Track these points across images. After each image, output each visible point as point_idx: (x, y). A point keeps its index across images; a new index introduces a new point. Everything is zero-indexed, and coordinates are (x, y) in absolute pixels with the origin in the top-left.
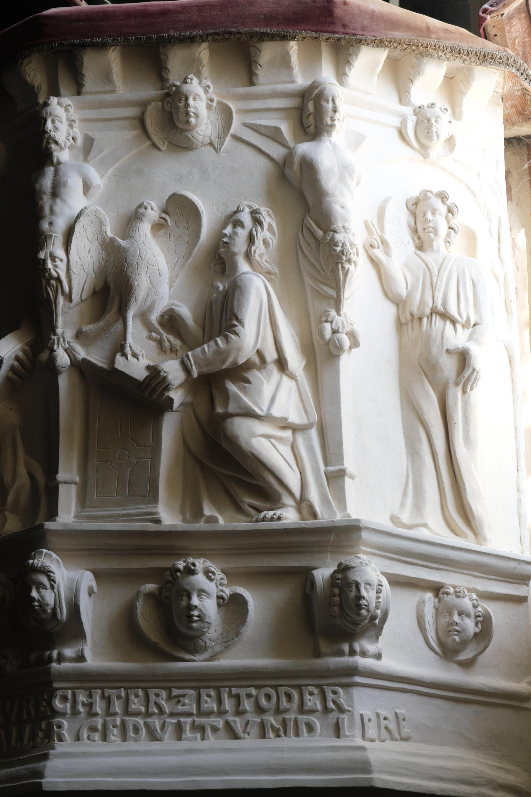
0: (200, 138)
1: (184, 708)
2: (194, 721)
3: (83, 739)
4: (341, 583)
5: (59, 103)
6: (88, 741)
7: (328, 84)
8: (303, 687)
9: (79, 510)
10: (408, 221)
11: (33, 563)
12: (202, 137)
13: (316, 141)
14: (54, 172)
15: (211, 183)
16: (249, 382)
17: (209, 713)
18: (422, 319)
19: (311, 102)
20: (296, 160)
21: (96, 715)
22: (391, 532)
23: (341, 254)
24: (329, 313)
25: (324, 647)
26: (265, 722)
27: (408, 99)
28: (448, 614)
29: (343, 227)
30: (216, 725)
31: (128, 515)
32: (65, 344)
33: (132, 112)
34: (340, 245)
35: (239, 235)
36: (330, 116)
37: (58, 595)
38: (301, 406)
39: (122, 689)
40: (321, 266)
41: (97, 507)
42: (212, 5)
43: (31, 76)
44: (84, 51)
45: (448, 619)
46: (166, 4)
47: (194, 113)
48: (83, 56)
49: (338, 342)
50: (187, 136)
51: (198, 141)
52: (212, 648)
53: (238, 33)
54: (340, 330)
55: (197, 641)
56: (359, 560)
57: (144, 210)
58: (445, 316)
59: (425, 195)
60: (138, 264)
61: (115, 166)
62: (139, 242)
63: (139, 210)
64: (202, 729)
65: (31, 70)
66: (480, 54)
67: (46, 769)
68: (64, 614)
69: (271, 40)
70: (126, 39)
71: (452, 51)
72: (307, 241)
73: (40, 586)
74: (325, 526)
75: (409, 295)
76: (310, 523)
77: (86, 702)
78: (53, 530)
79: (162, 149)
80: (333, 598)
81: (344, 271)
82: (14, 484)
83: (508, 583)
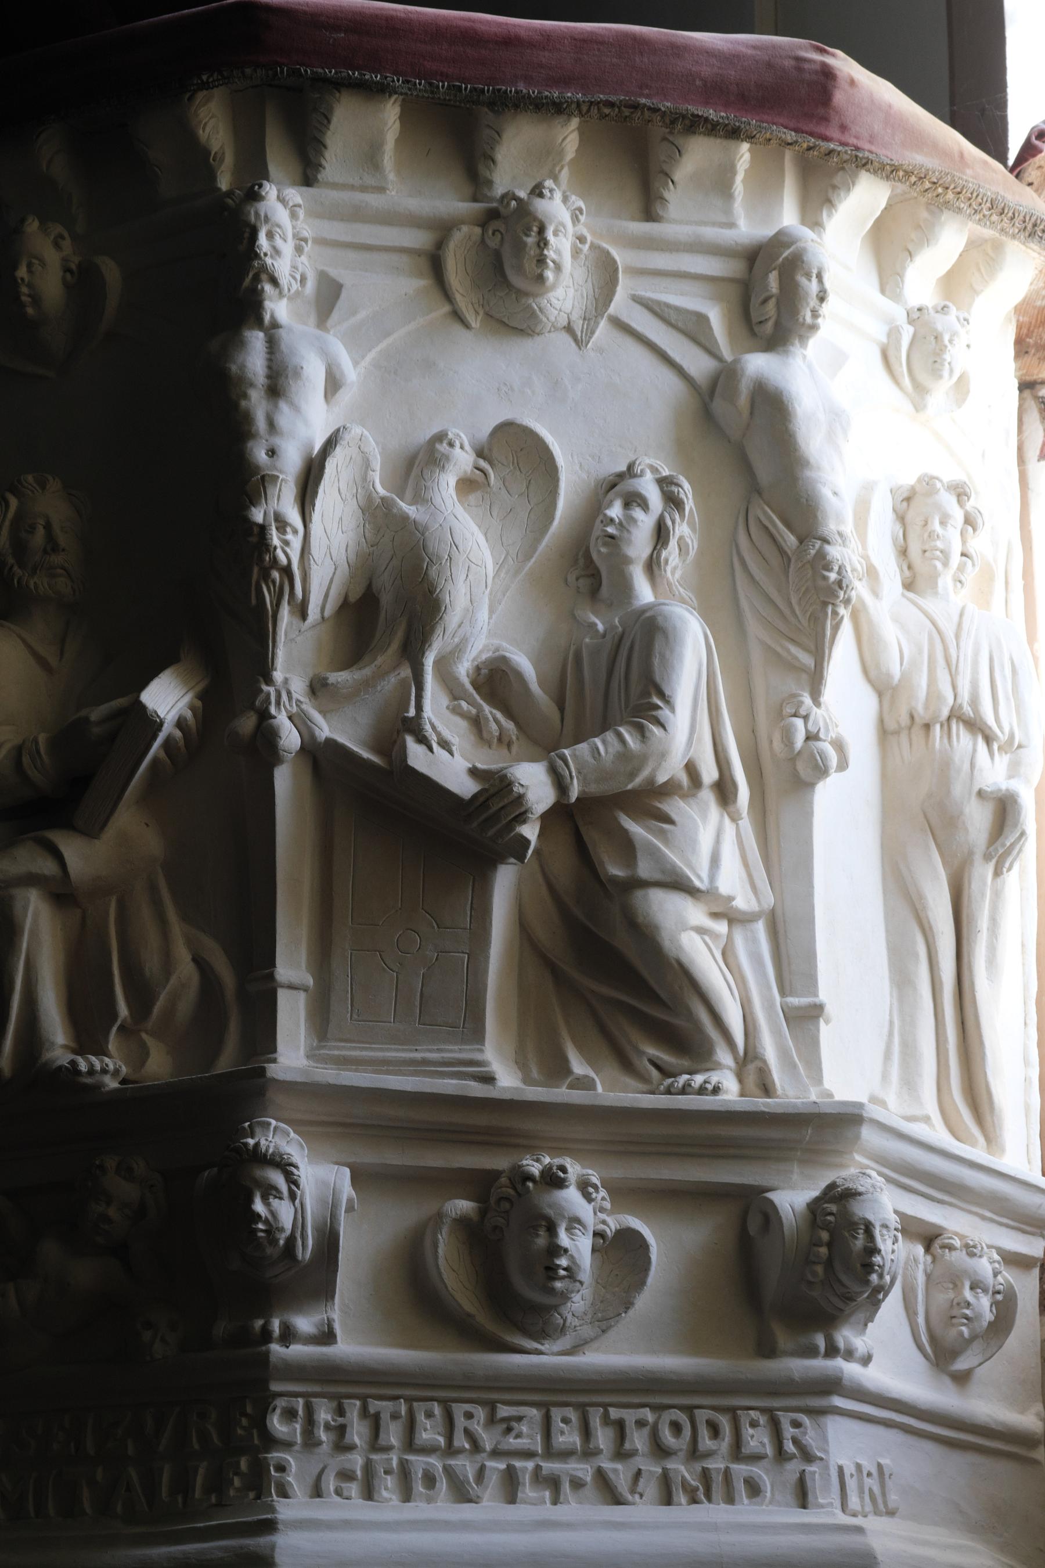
0: (553, 314)
1: (519, 1443)
2: (538, 1468)
3: (329, 1495)
4: (836, 1221)
5: (281, 198)
6: (337, 1499)
7: (810, 241)
8: (739, 1412)
9: (315, 1044)
10: (892, 532)
11: (257, 1144)
12: (557, 312)
13: (778, 353)
14: (266, 342)
15: (569, 408)
16: (670, 821)
17: (566, 1454)
18: (931, 728)
19: (774, 272)
20: (745, 388)
21: (351, 1448)
22: (901, 1129)
23: (837, 588)
24: (801, 698)
25: (783, 1339)
26: (671, 1475)
27: (898, 290)
28: (951, 1286)
29: (838, 532)
30: (581, 1476)
31: (425, 1062)
32: (291, 706)
33: (418, 239)
34: (836, 568)
35: (639, 523)
36: (812, 307)
37: (300, 1213)
38: (744, 875)
39: (402, 1400)
40: (790, 605)
41: (354, 1041)
42: (602, 43)
43: (208, 130)
44: (338, 95)
45: (951, 1295)
46: (511, 25)
47: (554, 262)
48: (334, 105)
49: (821, 758)
50: (529, 307)
51: (548, 319)
52: (576, 1331)
53: (649, 109)
54: (822, 735)
55: (552, 1315)
56: (869, 1181)
57: (447, 448)
58: (975, 726)
59: (929, 482)
60: (451, 558)
61: (378, 348)
62: (446, 514)
63: (438, 446)
64: (554, 1483)
65: (210, 116)
66: (1030, 219)
67: (277, 1550)
68: (306, 1250)
69: (708, 135)
70: (431, 84)
71: (992, 207)
72: (760, 553)
73: (269, 1191)
74: (801, 1111)
75: (905, 677)
76: (761, 1103)
77: (333, 1423)
78: (284, 1082)
79: (473, 325)
80: (816, 1249)
81: (835, 620)
82: (168, 980)
83: (1020, 1233)
